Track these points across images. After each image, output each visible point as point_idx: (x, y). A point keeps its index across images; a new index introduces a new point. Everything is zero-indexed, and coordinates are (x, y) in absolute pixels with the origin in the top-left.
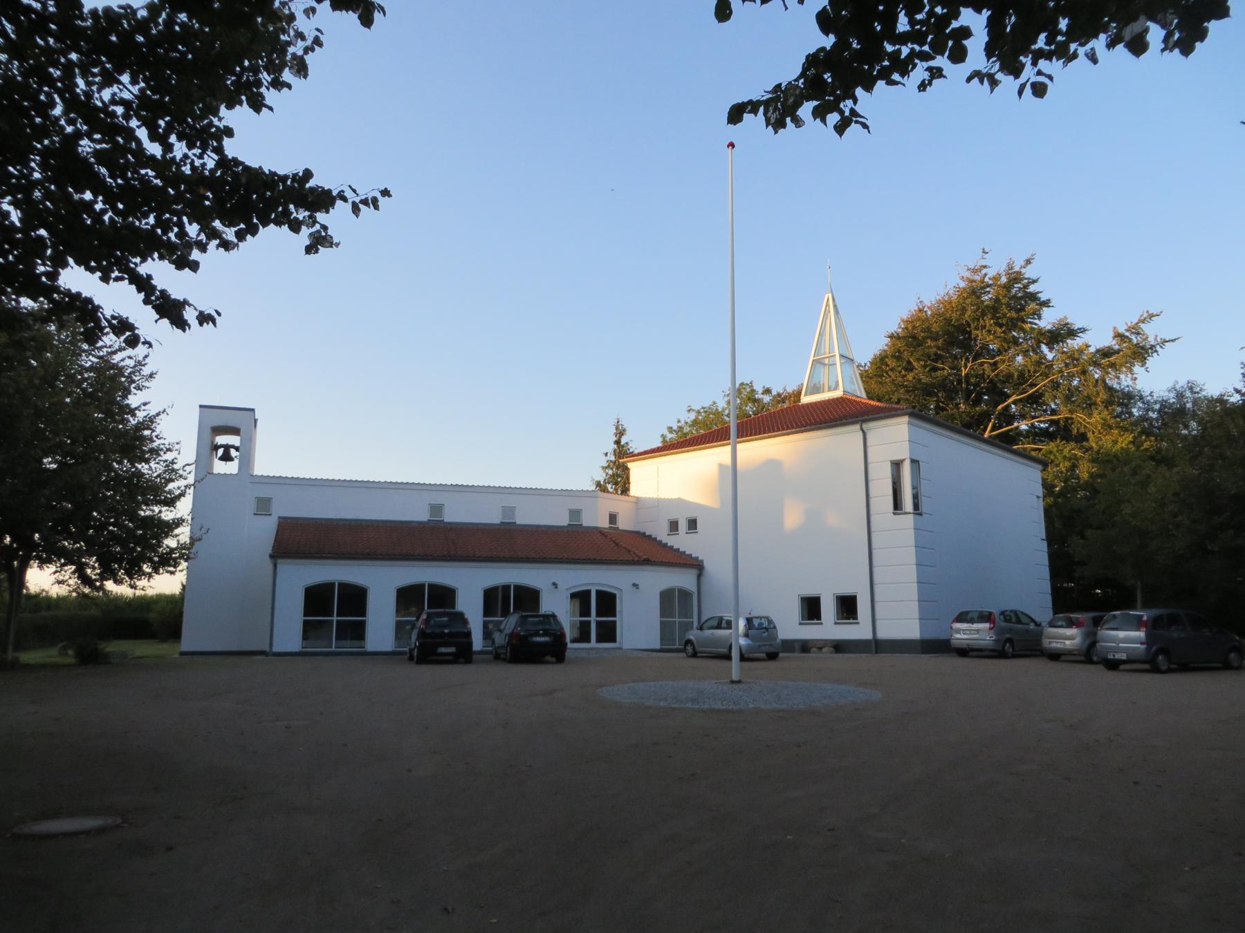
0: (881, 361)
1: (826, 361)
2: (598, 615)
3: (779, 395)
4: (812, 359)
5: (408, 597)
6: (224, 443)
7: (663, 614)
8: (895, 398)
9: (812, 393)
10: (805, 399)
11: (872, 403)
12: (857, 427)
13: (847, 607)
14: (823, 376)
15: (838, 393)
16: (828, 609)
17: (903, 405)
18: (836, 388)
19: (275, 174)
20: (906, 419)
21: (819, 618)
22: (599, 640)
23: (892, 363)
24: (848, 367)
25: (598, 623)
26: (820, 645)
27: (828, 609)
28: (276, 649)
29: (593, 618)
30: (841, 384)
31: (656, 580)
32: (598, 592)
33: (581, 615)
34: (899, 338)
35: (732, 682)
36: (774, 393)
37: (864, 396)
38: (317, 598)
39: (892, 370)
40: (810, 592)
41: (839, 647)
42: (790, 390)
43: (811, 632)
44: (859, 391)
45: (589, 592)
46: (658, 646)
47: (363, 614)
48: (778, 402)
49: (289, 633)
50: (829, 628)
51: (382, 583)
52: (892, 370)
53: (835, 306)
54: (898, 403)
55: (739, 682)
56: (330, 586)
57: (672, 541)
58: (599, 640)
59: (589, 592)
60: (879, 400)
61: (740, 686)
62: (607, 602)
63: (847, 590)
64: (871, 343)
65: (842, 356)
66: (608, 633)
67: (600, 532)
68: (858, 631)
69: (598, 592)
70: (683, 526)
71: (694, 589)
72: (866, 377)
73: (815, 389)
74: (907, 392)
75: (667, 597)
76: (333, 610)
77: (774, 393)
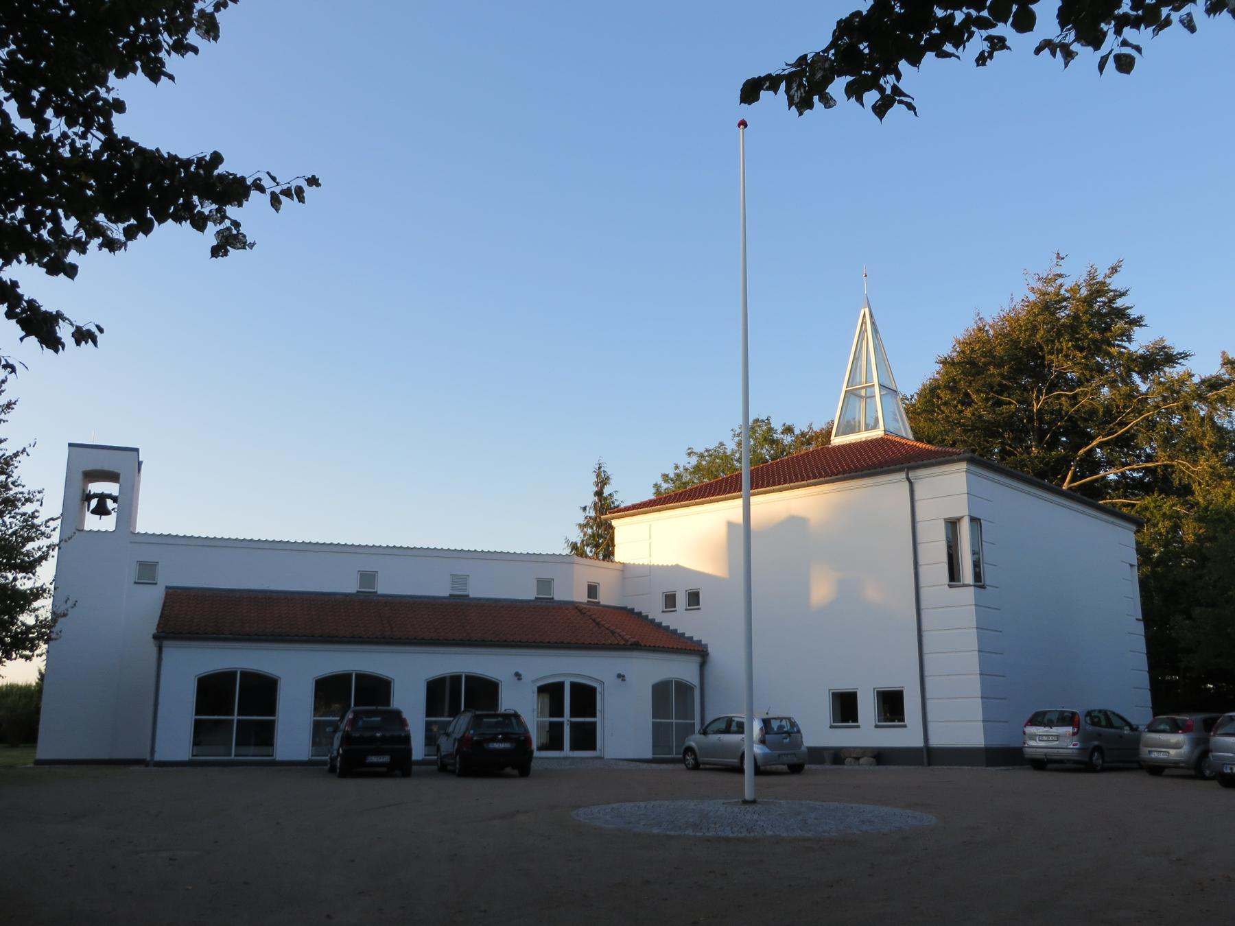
0: (931, 393)
1: (863, 392)
2: (572, 715)
3: (803, 435)
4: (844, 389)
5: (330, 690)
8: (949, 440)
9: (844, 434)
10: (836, 441)
11: (920, 445)
12: (902, 475)
13: (891, 705)
14: (859, 412)
15: (878, 433)
16: (867, 707)
17: (960, 449)
18: (875, 427)
20: (963, 466)
21: (855, 719)
23: (945, 395)
24: (889, 399)
27: (867, 707)
29: (567, 718)
30: (880, 422)
31: (648, 670)
34: (953, 364)
36: (797, 432)
37: (911, 436)
38: (213, 692)
39: (945, 404)
40: (844, 686)
41: (882, 756)
42: (816, 428)
43: (845, 738)
44: (904, 431)
45: (561, 685)
46: (649, 755)
48: (802, 444)
49: (175, 738)
50: (868, 732)
52: (945, 404)
53: (873, 324)
54: (953, 445)
59: (561, 685)
60: (929, 442)
62: (585, 698)
63: (890, 684)
64: (918, 371)
65: (881, 386)
66: (585, 738)
68: (905, 736)
70: (682, 601)
72: (912, 413)
73: (849, 428)
74: (965, 431)
75: (661, 692)
77: (797, 432)
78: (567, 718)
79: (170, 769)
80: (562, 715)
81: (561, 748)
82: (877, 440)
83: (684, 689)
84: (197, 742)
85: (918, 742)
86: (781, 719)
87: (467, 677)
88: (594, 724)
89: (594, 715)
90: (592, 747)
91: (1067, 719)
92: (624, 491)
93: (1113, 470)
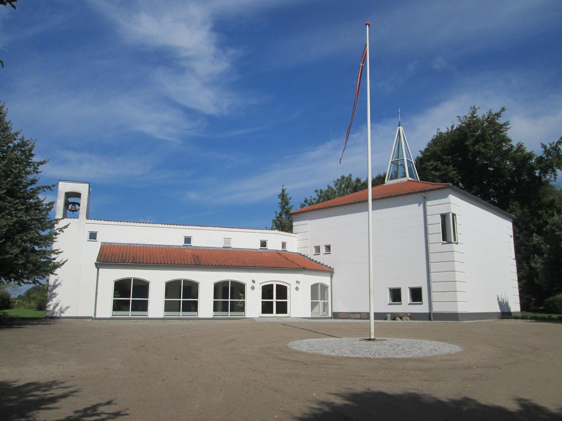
2: (277, 299)
4: (391, 160)
5: (172, 288)
6: (73, 201)
7: (312, 298)
13: (416, 295)
16: (406, 296)
19: (50, 267)
21: (400, 301)
22: (277, 313)
25: (277, 302)
26: (401, 316)
27: (406, 296)
28: (97, 316)
29: (274, 300)
31: (307, 280)
32: (277, 285)
33: (376, 314)
35: (370, 340)
38: (121, 287)
40: (395, 286)
41: (413, 316)
43: (396, 309)
45: (272, 285)
46: (310, 316)
47: (147, 296)
49: (105, 309)
50: (405, 305)
51: (157, 280)
55: (374, 339)
56: (129, 280)
57: (316, 258)
58: (277, 313)
59: (272, 285)
61: (375, 343)
62: (282, 291)
63: (416, 285)
66: (282, 308)
67: (278, 252)
68: (422, 308)
69: (277, 285)
70: (323, 250)
71: (329, 285)
75: (314, 288)
76: (130, 295)
78: (274, 300)
79: (79, 320)
80: (272, 298)
81: (272, 313)
82: (404, 182)
83: (324, 287)
84: (166, 310)
85: (427, 311)
86: (28, 283)
87: (278, 286)
88: (286, 302)
89: (286, 299)
90: (286, 313)
91: (61, 230)
92: (295, 205)
93: (535, 242)
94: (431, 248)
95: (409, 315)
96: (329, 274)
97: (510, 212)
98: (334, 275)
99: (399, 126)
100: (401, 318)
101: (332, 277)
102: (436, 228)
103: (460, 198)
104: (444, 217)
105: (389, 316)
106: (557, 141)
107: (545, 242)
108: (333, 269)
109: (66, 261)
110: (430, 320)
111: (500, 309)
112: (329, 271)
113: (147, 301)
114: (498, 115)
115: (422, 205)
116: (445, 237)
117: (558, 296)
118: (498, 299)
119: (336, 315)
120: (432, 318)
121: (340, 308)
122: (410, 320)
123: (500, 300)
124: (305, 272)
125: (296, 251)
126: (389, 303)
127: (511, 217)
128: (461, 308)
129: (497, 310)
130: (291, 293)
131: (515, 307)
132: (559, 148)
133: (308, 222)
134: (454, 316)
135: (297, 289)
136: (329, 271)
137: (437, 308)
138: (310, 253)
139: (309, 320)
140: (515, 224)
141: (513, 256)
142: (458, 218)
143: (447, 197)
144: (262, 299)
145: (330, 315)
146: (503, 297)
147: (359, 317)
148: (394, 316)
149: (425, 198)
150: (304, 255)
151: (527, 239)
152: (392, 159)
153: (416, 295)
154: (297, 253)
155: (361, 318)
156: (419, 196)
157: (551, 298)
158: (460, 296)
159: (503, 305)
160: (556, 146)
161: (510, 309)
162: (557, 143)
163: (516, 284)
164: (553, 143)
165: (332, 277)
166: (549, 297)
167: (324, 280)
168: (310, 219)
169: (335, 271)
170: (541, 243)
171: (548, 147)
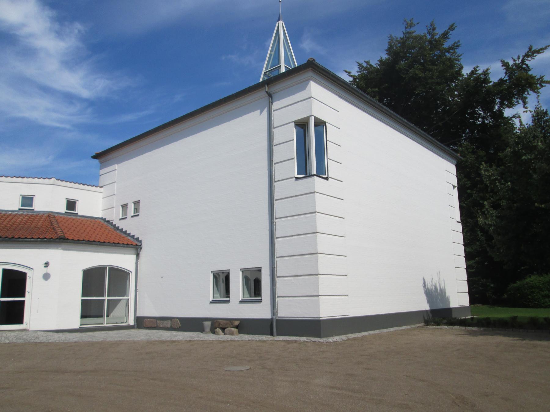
2: (108, 296)
4: (264, 71)
41: (245, 326)
57: (122, 225)
68: (260, 311)
83: (119, 277)
94: (280, 190)
95: (237, 323)
96: (133, 251)
97: (456, 151)
98: (143, 253)
99: (279, 20)
100: (223, 329)
101: (138, 255)
102: (288, 151)
103: (340, 97)
104: (302, 126)
105: (208, 324)
106: (524, 54)
107: (502, 178)
108: (141, 242)
109: (424, 280)
110: (272, 334)
111: (429, 302)
112: (134, 245)
113: (23, 303)
114: (445, 35)
115: (265, 112)
116: (304, 170)
117: (528, 280)
118: (425, 285)
119: (141, 323)
120: (275, 331)
121: (149, 310)
122: (240, 332)
123: (429, 286)
124: (64, 245)
125: (100, 215)
126: (241, 298)
127: (454, 157)
128: (328, 310)
129: (424, 305)
130: (33, 286)
131: (459, 297)
132: (527, 65)
133: (116, 166)
134: (312, 327)
135: (46, 277)
136: (134, 245)
137: (288, 310)
138: (115, 216)
139: (56, 336)
140: (459, 168)
141: (457, 216)
142: (331, 133)
143: (304, 88)
144: (82, 296)
145: (131, 322)
146: (436, 280)
147: (169, 326)
148: (218, 325)
149: (270, 95)
150: (108, 221)
151: (481, 194)
152: (267, 68)
153: (253, 285)
154: (102, 218)
155: (172, 329)
156: (261, 94)
157: (518, 283)
158: (325, 285)
159: (434, 294)
160: (523, 62)
161: (447, 301)
162: (524, 56)
163: (462, 262)
164: (518, 58)
165: (138, 255)
166: (515, 283)
167: (122, 260)
168: (118, 162)
169: (144, 245)
170: (496, 179)
171: (511, 63)
